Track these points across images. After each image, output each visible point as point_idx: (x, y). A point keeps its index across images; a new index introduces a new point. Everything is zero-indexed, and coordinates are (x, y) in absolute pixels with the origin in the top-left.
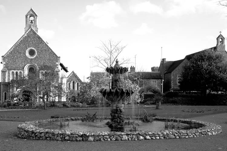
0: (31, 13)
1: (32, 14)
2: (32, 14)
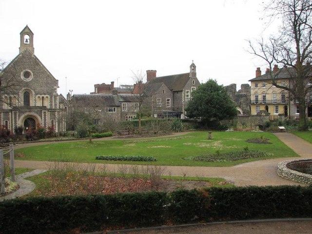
0: (27, 30)
1: (27, 31)
2: (27, 31)
